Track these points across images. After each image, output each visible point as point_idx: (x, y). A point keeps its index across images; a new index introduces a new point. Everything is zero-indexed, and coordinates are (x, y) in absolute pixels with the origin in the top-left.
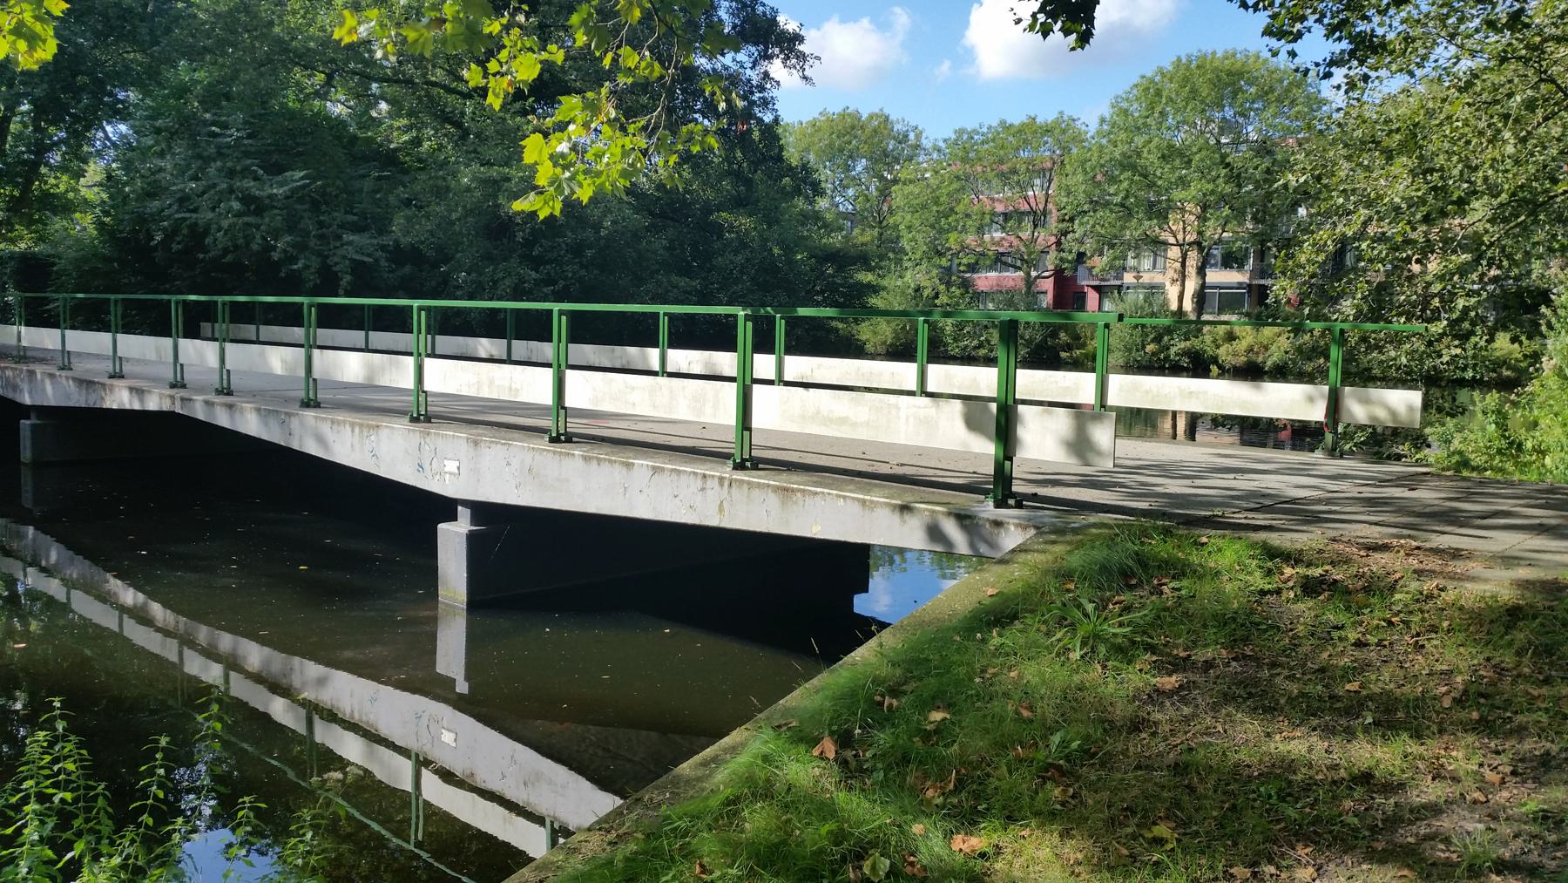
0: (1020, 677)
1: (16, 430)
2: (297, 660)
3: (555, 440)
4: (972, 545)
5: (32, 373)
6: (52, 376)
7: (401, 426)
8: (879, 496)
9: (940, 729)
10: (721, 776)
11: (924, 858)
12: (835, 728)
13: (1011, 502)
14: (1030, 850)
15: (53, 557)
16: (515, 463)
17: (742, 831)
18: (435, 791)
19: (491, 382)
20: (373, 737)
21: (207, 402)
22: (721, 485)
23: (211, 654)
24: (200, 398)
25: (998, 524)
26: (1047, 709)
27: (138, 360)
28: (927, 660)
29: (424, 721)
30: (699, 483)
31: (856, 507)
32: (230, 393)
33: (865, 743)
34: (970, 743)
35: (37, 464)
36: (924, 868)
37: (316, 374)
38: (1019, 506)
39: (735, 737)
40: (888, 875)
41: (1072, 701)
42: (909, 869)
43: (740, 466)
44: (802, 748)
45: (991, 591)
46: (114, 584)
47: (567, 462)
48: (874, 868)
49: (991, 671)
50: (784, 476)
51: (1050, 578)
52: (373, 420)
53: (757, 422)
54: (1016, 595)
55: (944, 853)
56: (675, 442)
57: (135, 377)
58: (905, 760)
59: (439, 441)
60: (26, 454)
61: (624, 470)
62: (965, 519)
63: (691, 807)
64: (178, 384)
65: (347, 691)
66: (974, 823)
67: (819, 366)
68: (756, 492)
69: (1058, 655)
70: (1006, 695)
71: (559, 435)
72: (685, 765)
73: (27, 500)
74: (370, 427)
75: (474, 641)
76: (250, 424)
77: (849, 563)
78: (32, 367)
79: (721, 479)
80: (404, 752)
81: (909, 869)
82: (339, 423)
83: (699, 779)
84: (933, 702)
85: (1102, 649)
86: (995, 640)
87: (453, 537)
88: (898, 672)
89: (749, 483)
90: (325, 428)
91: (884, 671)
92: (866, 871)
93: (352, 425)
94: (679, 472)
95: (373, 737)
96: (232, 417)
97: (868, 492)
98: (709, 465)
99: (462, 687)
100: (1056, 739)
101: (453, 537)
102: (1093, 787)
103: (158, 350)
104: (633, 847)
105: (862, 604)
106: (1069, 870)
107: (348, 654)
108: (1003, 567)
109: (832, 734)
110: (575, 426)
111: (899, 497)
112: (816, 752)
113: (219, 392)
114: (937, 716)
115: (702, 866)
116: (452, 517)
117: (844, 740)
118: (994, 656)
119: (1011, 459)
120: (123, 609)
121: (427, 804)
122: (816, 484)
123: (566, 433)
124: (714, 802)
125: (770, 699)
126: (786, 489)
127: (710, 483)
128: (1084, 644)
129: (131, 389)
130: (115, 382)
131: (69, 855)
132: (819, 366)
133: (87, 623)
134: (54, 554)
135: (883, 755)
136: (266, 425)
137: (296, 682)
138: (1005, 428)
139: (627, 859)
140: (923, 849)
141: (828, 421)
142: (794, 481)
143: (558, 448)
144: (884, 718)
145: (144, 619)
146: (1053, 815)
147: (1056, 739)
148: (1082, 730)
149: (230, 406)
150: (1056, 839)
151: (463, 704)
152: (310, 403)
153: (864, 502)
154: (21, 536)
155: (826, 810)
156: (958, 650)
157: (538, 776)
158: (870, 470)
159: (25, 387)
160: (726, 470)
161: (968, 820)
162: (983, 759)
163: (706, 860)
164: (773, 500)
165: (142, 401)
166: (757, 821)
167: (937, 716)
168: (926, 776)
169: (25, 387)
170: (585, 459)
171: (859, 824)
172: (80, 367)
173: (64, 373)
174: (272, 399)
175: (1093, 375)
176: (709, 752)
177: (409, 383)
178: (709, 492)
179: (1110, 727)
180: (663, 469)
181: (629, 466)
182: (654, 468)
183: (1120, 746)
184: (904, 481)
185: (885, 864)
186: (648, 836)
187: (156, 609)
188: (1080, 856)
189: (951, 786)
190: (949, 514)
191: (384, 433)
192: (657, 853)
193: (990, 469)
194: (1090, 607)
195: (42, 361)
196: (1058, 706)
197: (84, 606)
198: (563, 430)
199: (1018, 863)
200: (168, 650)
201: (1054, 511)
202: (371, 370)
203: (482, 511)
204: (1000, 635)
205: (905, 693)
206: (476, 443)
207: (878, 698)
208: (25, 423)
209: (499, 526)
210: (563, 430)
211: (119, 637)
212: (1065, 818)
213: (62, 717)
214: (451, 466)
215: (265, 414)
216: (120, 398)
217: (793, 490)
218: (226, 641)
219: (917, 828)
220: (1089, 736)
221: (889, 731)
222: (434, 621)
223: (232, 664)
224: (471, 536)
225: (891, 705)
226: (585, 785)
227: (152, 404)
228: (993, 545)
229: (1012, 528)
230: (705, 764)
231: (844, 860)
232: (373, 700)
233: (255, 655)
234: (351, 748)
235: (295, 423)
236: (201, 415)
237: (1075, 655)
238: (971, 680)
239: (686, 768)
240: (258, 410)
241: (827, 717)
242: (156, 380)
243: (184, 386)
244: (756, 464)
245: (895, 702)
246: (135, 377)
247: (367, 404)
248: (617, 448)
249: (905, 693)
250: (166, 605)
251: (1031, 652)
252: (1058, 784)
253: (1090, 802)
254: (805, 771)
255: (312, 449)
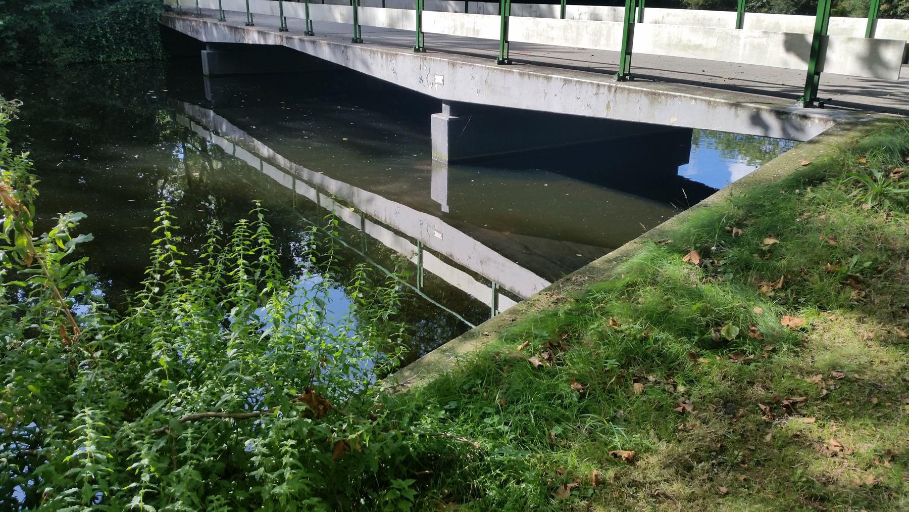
0: (828, 218)
1: (199, 56)
2: (355, 189)
3: (501, 63)
4: (784, 130)
5: (205, 23)
6: (216, 25)
7: (409, 54)
8: (720, 98)
9: (772, 250)
10: (621, 268)
11: (761, 328)
12: (698, 245)
13: (816, 103)
14: (836, 329)
15: (224, 128)
16: (477, 77)
17: (638, 303)
18: (431, 264)
19: (462, 26)
20: (398, 233)
21: (301, 40)
22: (610, 91)
23: (310, 183)
24: (297, 37)
25: (805, 117)
26: (847, 241)
27: (260, 15)
28: (762, 206)
29: (425, 225)
30: (595, 90)
31: (704, 106)
32: (312, 35)
33: (719, 255)
34: (791, 259)
35: (211, 76)
36: (762, 334)
37: (360, 22)
38: (821, 106)
39: (628, 246)
40: (738, 337)
41: (865, 236)
42: (751, 334)
43: (622, 79)
44: (676, 256)
45: (804, 163)
46: (258, 144)
47: (509, 76)
48: (728, 332)
49: (806, 214)
50: (653, 85)
51: (849, 154)
52: (393, 51)
53: (636, 49)
54: (823, 166)
55: (777, 327)
56: (576, 64)
57: (259, 25)
58: (747, 267)
59: (432, 64)
60: (206, 70)
61: (546, 82)
62: (780, 114)
63: (604, 285)
64: (284, 29)
65: (382, 207)
66: (797, 309)
67: (668, 15)
68: (633, 96)
69: (855, 205)
70: (819, 230)
71: (504, 59)
72: (596, 261)
73: (209, 97)
74: (392, 55)
75: (452, 182)
76: (325, 53)
77: (678, 141)
78: (205, 20)
79: (610, 87)
80: (413, 241)
81: (751, 334)
82: (374, 52)
83: (605, 270)
84: (769, 231)
85: (887, 203)
86: (809, 193)
87: (440, 122)
88: (741, 212)
89: (629, 90)
90: (367, 56)
91: (733, 211)
92: (723, 333)
93: (382, 53)
94: (582, 82)
95: (398, 233)
96: (315, 49)
97: (712, 96)
98: (601, 78)
99: (445, 209)
100: (855, 259)
101: (440, 122)
102: (880, 292)
103: (271, 9)
104: (568, 306)
105: (686, 171)
106: (863, 343)
107: (381, 188)
108: (812, 146)
109: (696, 248)
110: (513, 54)
111: (730, 99)
112: (686, 259)
113: (307, 34)
114: (770, 241)
115: (613, 321)
116: (439, 110)
117: (705, 253)
118: (809, 204)
119: (818, 74)
120: (263, 159)
121: (425, 270)
122: (674, 90)
123: (508, 59)
124: (619, 285)
125: (652, 225)
126: (655, 94)
127: (602, 90)
128: (874, 199)
129: (259, 32)
130: (250, 28)
131: (265, 290)
132: (668, 15)
133: (245, 165)
134: (225, 126)
135: (731, 264)
136: (334, 53)
137: (356, 201)
138: (817, 50)
139: (566, 313)
140: (761, 323)
141: (687, 47)
142: (660, 88)
143: (503, 67)
144: (737, 241)
145: (270, 161)
146: (852, 308)
147: (855, 259)
148: (873, 256)
149: (314, 42)
150: (854, 322)
151: (446, 218)
152: (357, 41)
153: (709, 102)
154: (206, 116)
155: (696, 295)
156: (784, 200)
157: (489, 259)
158: (710, 81)
159: (203, 31)
160: (613, 82)
161: (795, 306)
162: (802, 270)
163: (615, 318)
164: (645, 100)
165: (265, 39)
166: (648, 297)
167: (770, 241)
168: (762, 279)
169: (203, 31)
170: (520, 74)
171: (718, 305)
172: (230, 19)
173: (222, 23)
174: (335, 37)
175: (867, 19)
176: (611, 255)
177: (413, 27)
178: (600, 95)
179: (893, 254)
180: (571, 81)
181: (548, 79)
182: (565, 80)
183: (899, 267)
184: (735, 89)
185: (736, 331)
186: (577, 301)
187: (281, 159)
188: (871, 335)
189: (780, 285)
190: (771, 111)
191: (400, 58)
192: (584, 311)
193: (802, 83)
194: (879, 175)
195: (209, 16)
196: (855, 239)
197: (242, 154)
198: (506, 55)
199: (826, 336)
200: (285, 181)
201: (849, 111)
202: (392, 20)
203: (457, 107)
204: (812, 191)
205: (746, 226)
206: (454, 65)
207: (728, 228)
208: (204, 52)
209: (467, 115)
210: (506, 55)
211: (259, 174)
212: (864, 309)
213: (261, 212)
214: (439, 79)
215: (334, 47)
216: (253, 38)
217: (659, 94)
218: (318, 177)
219: (757, 310)
220: (876, 259)
221: (736, 249)
222: (430, 171)
223: (321, 189)
224: (451, 123)
225: (737, 233)
226: (515, 266)
227: (271, 41)
228: (800, 129)
229: (817, 121)
230: (609, 261)
231: (708, 325)
232: (397, 213)
233: (333, 185)
234: (386, 239)
235: (350, 52)
236: (297, 47)
237: (868, 206)
238: (794, 219)
239: (597, 262)
240: (329, 44)
241: (693, 239)
242: (271, 27)
243: (287, 30)
244: (633, 78)
245: (740, 231)
246: (259, 25)
247: (390, 40)
248: (540, 68)
249: (746, 226)
250: (285, 156)
251: (838, 202)
252: (854, 288)
253: (876, 301)
254: (683, 269)
255: (360, 69)
